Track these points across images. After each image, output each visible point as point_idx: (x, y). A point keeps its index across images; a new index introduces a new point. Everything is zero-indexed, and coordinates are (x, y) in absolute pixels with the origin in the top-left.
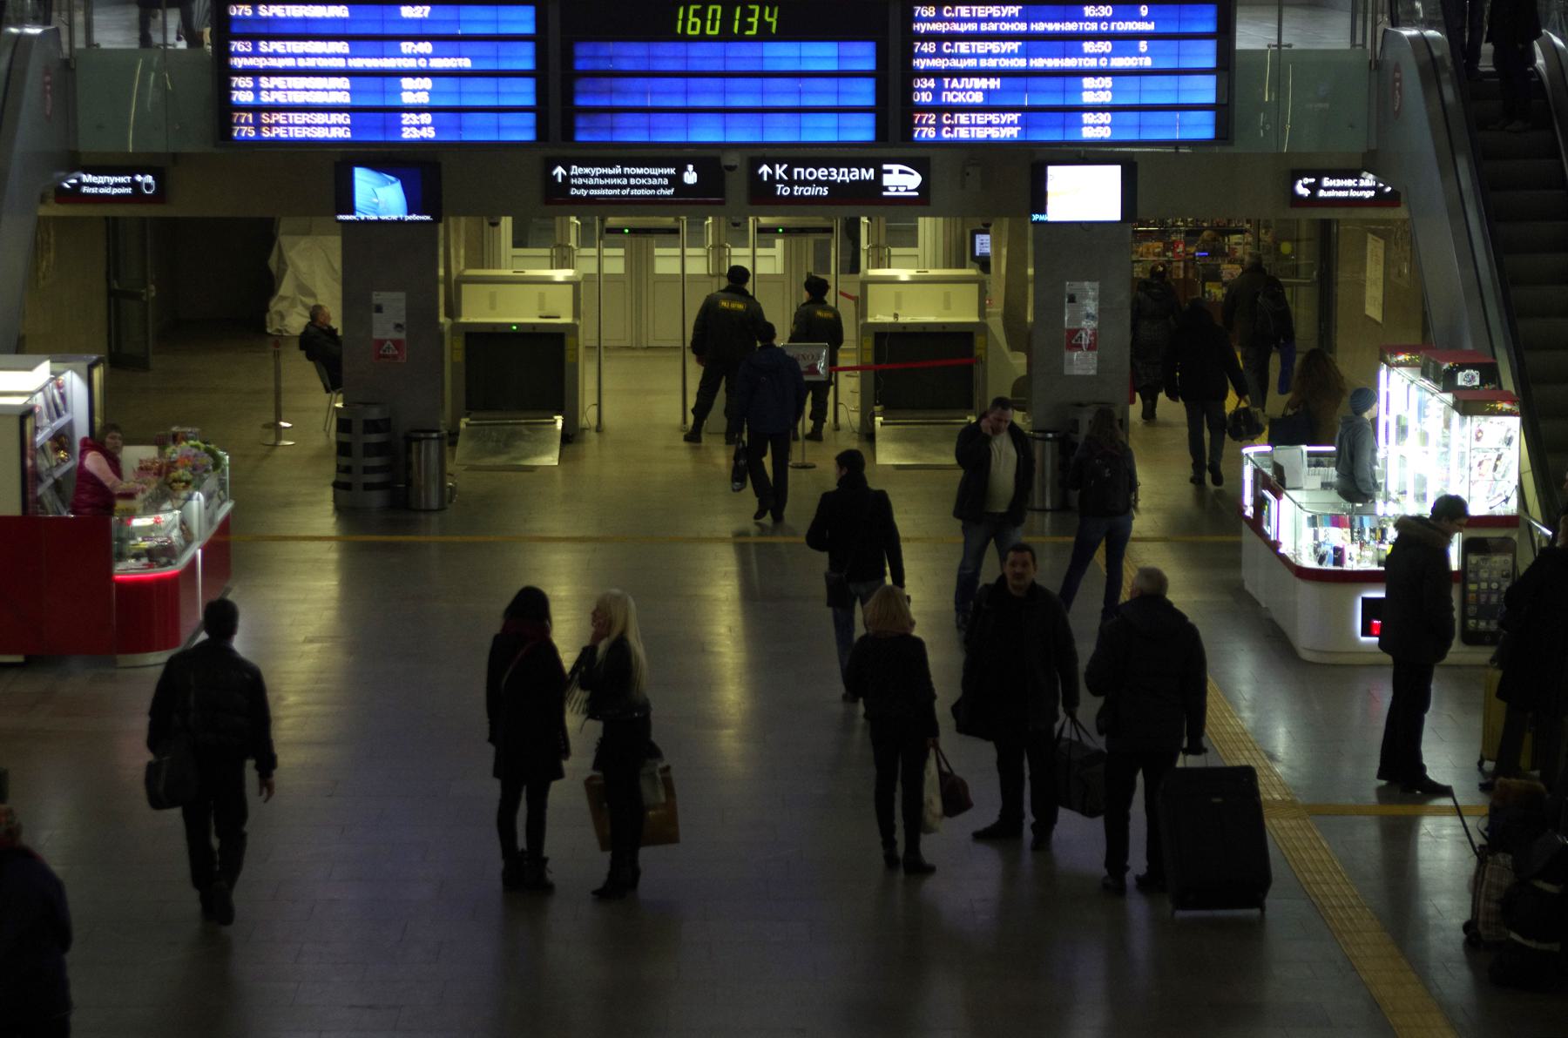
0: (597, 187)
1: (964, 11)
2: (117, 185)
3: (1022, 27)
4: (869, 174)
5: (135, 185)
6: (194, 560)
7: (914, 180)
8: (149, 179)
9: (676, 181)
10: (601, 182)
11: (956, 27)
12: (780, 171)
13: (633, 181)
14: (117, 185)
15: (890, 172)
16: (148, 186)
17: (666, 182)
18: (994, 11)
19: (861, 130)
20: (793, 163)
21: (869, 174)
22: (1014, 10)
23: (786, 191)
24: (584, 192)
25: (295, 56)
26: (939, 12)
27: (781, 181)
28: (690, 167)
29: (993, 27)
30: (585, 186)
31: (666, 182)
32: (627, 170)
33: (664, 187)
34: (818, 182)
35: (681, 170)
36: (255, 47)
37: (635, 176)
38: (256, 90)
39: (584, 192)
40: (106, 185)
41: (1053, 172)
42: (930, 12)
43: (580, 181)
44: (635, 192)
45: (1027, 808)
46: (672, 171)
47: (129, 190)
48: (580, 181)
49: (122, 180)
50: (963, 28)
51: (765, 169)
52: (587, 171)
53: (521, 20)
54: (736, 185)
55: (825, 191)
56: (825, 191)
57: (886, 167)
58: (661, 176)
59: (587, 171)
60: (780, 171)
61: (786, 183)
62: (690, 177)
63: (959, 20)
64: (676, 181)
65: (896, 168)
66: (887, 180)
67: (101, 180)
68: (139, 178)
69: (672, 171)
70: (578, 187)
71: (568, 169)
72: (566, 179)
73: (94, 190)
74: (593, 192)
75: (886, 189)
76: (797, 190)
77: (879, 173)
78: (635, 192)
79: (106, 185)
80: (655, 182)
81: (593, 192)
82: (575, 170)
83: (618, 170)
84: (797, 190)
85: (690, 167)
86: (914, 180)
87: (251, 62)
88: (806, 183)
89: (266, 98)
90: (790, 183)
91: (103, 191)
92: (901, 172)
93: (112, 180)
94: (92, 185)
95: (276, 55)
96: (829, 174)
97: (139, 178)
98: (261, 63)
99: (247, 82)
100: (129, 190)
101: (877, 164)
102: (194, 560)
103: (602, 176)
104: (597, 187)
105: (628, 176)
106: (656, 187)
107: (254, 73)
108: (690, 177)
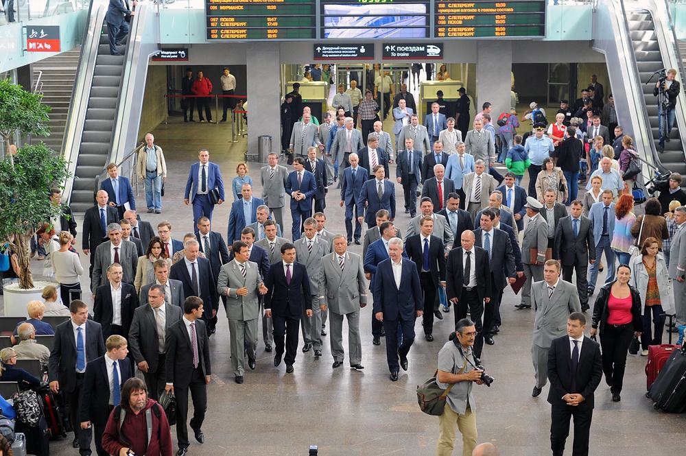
0: (331, 54)
1: (455, 5)
2: (173, 55)
3: (475, 10)
4: (422, 49)
5: (178, 54)
6: (596, 197)
7: (438, 51)
8: (183, 52)
9: (358, 52)
11: (452, 11)
12: (392, 48)
13: (343, 52)
14: (173, 55)
16: (183, 55)
18: (465, 5)
19: (419, 34)
20: (397, 45)
21: (422, 49)
22: (472, 5)
23: (395, 55)
24: (327, 56)
25: (460, 8)
27: (393, 51)
28: (363, 47)
29: (465, 10)
30: (327, 54)
31: (354, 52)
32: (342, 48)
34: (406, 52)
35: (360, 48)
38: (446, 20)
39: (327, 56)
40: (169, 55)
42: (443, 6)
44: (344, 55)
46: (356, 48)
47: (176, 56)
48: (326, 52)
49: (174, 53)
50: (455, 11)
51: (388, 47)
52: (328, 48)
54: (378, 52)
55: (408, 55)
56: (408, 55)
57: (428, 46)
59: (328, 48)
60: (392, 48)
62: (363, 50)
63: (454, 8)
64: (358, 52)
66: (428, 51)
67: (168, 53)
68: (180, 52)
69: (356, 48)
70: (325, 54)
72: (321, 51)
74: (330, 56)
76: (399, 54)
77: (426, 48)
78: (344, 55)
79: (169, 55)
80: (351, 52)
81: (330, 56)
82: (324, 48)
83: (338, 48)
84: (399, 54)
85: (363, 47)
86: (438, 51)
87: (445, 11)
89: (451, 22)
90: (396, 52)
91: (168, 57)
93: (171, 53)
94: (165, 55)
95: (454, 8)
97: (180, 52)
98: (448, 11)
99: (443, 18)
100: (176, 56)
101: (425, 45)
102: (596, 197)
103: (333, 50)
104: (331, 54)
105: (342, 50)
106: (351, 54)
107: (446, 15)
108: (363, 50)
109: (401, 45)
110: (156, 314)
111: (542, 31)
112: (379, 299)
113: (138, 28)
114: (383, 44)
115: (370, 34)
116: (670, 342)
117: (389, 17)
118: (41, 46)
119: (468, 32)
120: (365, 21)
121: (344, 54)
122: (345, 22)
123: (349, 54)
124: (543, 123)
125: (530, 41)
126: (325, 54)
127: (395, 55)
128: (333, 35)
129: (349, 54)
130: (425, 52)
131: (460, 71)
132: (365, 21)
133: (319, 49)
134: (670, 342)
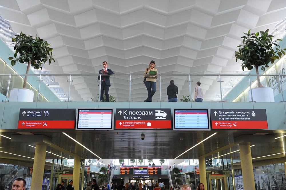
5: (43, 114)
9: (250, 115)
10: (228, 116)
14: (38, 114)
15: (157, 112)
16: (47, 114)
17: (247, 116)
23: (127, 118)
26: (227, 123)
28: (253, 112)
31: (247, 116)
33: (247, 117)
35: (251, 112)
36: (227, 123)
37: (238, 114)
41: (156, 113)
43: (222, 116)
45: (37, 123)
48: (222, 116)
53: (26, 126)
54: (141, 177)
58: (246, 114)
61: (127, 116)
65: (159, 111)
66: (157, 115)
70: (222, 117)
71: (218, 112)
72: (218, 115)
73: (30, 116)
74: (226, 119)
75: (156, 117)
77: (154, 113)
81: (226, 119)
82: (220, 112)
85: (253, 112)
88: (132, 116)
90: (128, 116)
92: (161, 112)
96: (139, 113)
103: (228, 114)
105: (236, 114)
106: (245, 117)
108: (254, 115)
111: (161, 173)
112: (31, 128)
113: (50, 74)
114: (78, 109)
115: (140, 173)
117: (142, 171)
119: (152, 173)
120: (139, 172)
121: (238, 117)
122: (137, 172)
123: (243, 117)
125: (146, 65)
126: (222, 117)
127: (127, 118)
128: (135, 173)
129: (243, 117)
132: (139, 172)
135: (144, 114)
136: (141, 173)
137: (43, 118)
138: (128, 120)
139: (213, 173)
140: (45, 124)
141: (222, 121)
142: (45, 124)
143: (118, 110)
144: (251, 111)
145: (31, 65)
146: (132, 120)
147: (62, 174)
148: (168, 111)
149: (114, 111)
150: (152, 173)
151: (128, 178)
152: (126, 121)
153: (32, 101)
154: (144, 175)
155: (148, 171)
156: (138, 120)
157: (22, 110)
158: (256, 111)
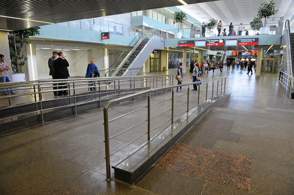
4: (218, 41)
9: (252, 40)
12: (209, 41)
21: (218, 41)
60: (209, 41)
64: (252, 40)
65: (221, 40)
66: (219, 41)
76: (211, 42)
82: (242, 39)
83: (246, 39)
84: (211, 42)
90: (210, 42)
108: (254, 40)
109: (212, 40)
110: (24, 104)
116: (119, 88)
118: (105, 38)
124: (243, 51)
128: (242, 55)
130: (219, 42)
131: (141, 54)
133: (240, 40)
134: (119, 88)
135: (215, 41)
136: (247, 55)
137: (185, 43)
138: (210, 43)
139: (268, 57)
140: (186, 45)
141: (242, 42)
142: (186, 45)
143: (239, 39)
144: (253, 39)
145: (36, 36)
146: (212, 43)
147: (194, 57)
148: (223, 40)
149: (206, 40)
150: (254, 55)
151: (237, 57)
152: (210, 43)
153: (275, 34)
154: (249, 56)
155: (251, 54)
156: (213, 43)
157: (179, 41)
158: (255, 39)
